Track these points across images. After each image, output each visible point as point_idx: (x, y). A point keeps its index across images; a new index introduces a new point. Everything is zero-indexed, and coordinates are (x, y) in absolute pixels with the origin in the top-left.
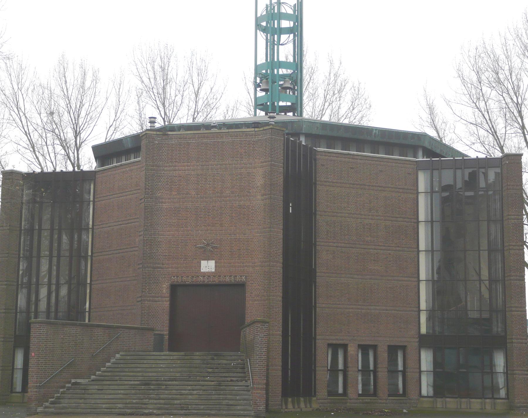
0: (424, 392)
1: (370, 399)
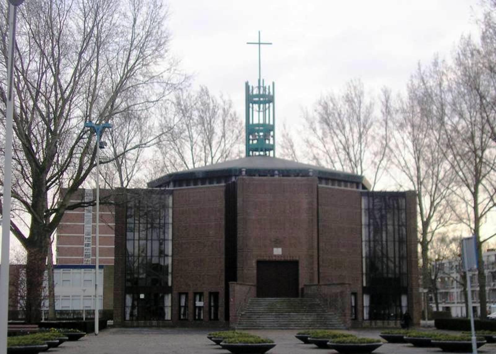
0: (365, 318)
1: (76, 332)
